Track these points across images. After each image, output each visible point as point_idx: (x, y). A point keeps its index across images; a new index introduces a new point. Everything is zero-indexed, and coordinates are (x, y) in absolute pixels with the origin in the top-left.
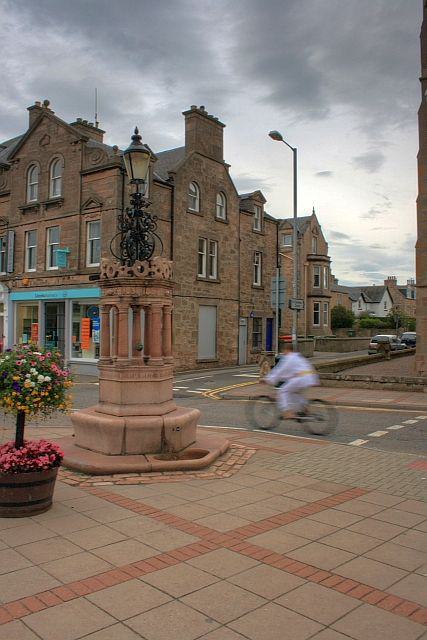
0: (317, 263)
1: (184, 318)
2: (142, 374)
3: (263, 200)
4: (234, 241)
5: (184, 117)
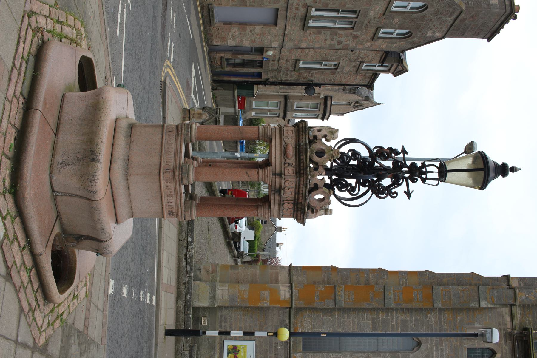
0: (322, 107)
2: (172, 199)
3: (396, 74)
4: (352, 44)
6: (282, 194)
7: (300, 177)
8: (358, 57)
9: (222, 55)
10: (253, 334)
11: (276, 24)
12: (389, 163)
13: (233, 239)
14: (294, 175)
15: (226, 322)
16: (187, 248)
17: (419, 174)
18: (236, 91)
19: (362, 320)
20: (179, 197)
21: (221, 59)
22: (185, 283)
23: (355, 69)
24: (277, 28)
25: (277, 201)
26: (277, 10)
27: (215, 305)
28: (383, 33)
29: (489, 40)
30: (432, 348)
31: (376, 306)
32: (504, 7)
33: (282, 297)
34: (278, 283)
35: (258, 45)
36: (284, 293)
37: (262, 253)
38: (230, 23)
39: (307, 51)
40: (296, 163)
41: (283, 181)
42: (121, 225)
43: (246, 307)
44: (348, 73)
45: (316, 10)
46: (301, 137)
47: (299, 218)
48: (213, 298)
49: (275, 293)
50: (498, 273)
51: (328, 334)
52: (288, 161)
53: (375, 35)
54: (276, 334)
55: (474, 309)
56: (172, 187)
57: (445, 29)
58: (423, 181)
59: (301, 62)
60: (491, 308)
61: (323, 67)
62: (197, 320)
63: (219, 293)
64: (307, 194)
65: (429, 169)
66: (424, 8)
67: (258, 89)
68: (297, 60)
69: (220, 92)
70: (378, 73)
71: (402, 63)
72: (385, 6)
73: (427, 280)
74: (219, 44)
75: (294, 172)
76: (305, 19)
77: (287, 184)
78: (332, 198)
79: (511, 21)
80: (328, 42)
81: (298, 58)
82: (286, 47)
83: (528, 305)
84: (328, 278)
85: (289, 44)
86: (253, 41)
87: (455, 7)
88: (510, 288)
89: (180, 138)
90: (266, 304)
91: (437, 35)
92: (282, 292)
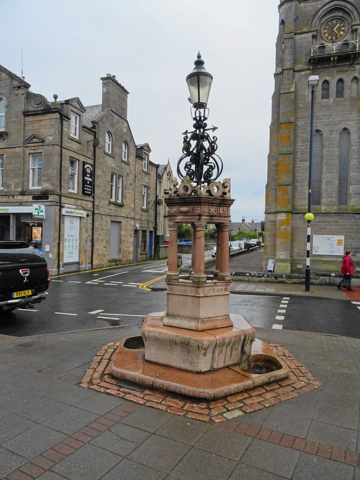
1: (102, 230)
3: (149, 150)
4: (132, 177)
5: (101, 81)
6: (213, 215)
7: (201, 202)
8: (140, 173)
9: (139, 254)
10: (309, 236)
11: (120, 222)
12: (193, 143)
13: (249, 248)
14: (200, 206)
15: (300, 253)
16: (253, 276)
17: (201, 122)
18: (161, 246)
19: (301, 168)
21: (142, 254)
22: (276, 278)
23: (147, 175)
24: (122, 222)
25: (218, 218)
26: (112, 221)
27: (289, 260)
28: (125, 158)
29: (128, 93)
30: (321, 122)
31: (292, 159)
32: (108, 84)
33: (285, 218)
34: (276, 220)
35: (133, 233)
36: (282, 217)
37: (257, 231)
38: (120, 249)
39: (136, 204)
40: (192, 205)
41: (204, 214)
42: (234, 323)
43: (291, 241)
44: (149, 180)
45: (111, 198)
46: (175, 202)
47: (230, 203)
48: (284, 261)
49: (282, 223)
50: (272, 81)
51: (309, 189)
52: (191, 211)
53: (126, 163)
54: (309, 221)
55: (295, 96)
56: (209, 288)
57: (122, 120)
58: (205, 119)
59: (143, 207)
60: (295, 85)
61: (146, 194)
62: (299, 271)
63: (282, 257)
64: (213, 197)
65: (198, 115)
66: (109, 133)
67: (160, 233)
68: (142, 210)
69: (161, 255)
70: (149, 161)
71: (143, 147)
72: (108, 157)
73: (277, 126)
74: (132, 256)
75: (198, 206)
76: (116, 204)
77: (206, 211)
78: (216, 181)
79: (116, 79)
80: (130, 191)
81: (141, 209)
82: (133, 216)
83: (294, 60)
84: (274, 187)
85: (132, 215)
86: (131, 236)
87: (108, 114)
88: (282, 73)
89: (175, 283)
90: (289, 228)
91: (125, 125)
92: (282, 218)
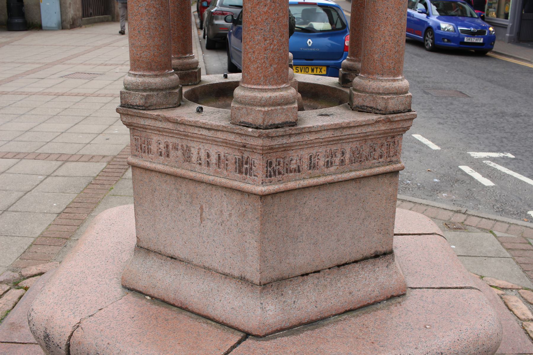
2: (198, 150)
20: (182, 128)
56: (163, 140)
